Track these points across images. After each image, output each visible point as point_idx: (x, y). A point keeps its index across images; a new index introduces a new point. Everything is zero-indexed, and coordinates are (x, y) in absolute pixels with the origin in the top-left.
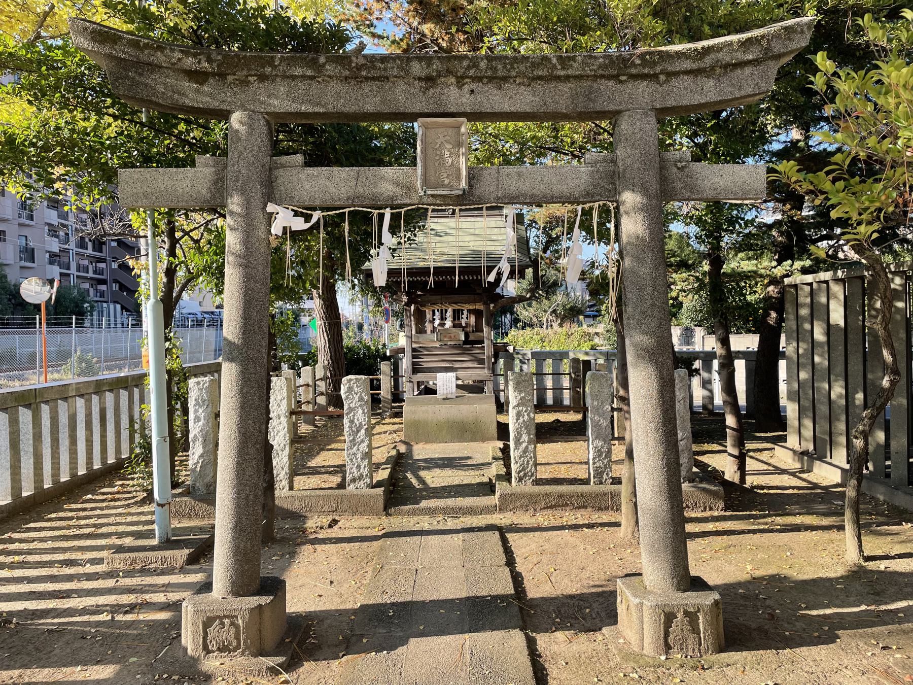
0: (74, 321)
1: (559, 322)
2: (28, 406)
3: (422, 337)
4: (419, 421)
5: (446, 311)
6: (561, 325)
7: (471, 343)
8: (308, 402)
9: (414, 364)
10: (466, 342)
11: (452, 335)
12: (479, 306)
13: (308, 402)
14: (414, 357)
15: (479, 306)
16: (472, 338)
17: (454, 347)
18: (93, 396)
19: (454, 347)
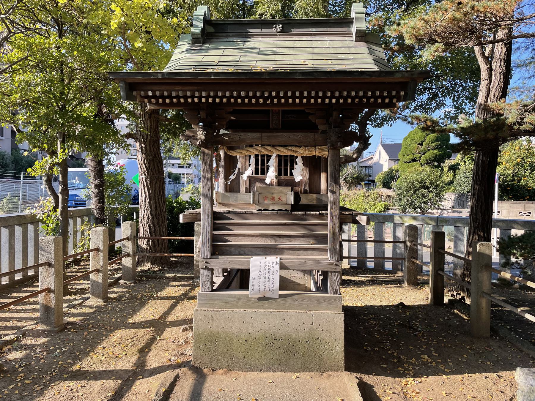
0: (22, 175)
1: (348, 186)
2: (20, 225)
3: (232, 197)
4: (218, 335)
5: (269, 157)
6: (349, 189)
7: (304, 207)
8: (98, 271)
9: (214, 239)
10: (297, 206)
11: (277, 198)
12: (321, 152)
13: (98, 271)
14: (215, 227)
15: (321, 152)
16: (304, 200)
17: (280, 213)
18: (29, 225)
19: (280, 213)
